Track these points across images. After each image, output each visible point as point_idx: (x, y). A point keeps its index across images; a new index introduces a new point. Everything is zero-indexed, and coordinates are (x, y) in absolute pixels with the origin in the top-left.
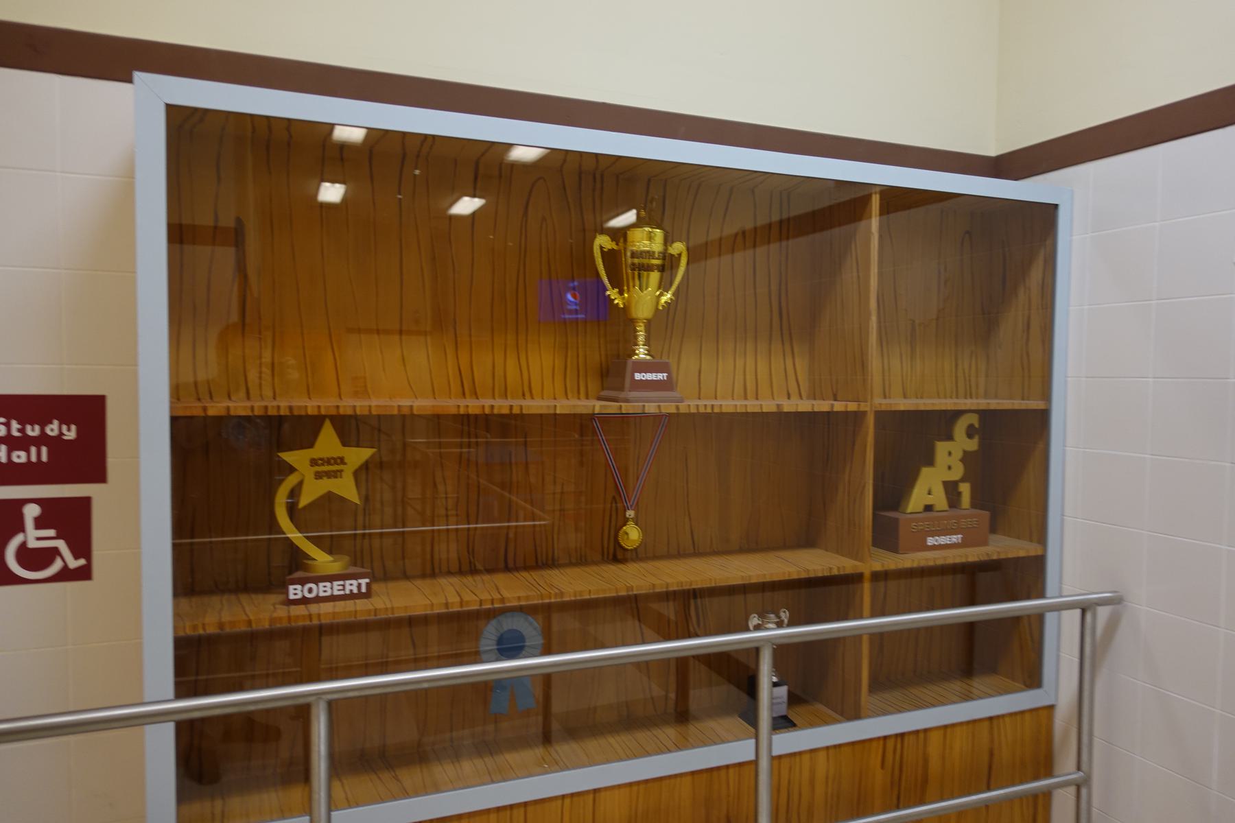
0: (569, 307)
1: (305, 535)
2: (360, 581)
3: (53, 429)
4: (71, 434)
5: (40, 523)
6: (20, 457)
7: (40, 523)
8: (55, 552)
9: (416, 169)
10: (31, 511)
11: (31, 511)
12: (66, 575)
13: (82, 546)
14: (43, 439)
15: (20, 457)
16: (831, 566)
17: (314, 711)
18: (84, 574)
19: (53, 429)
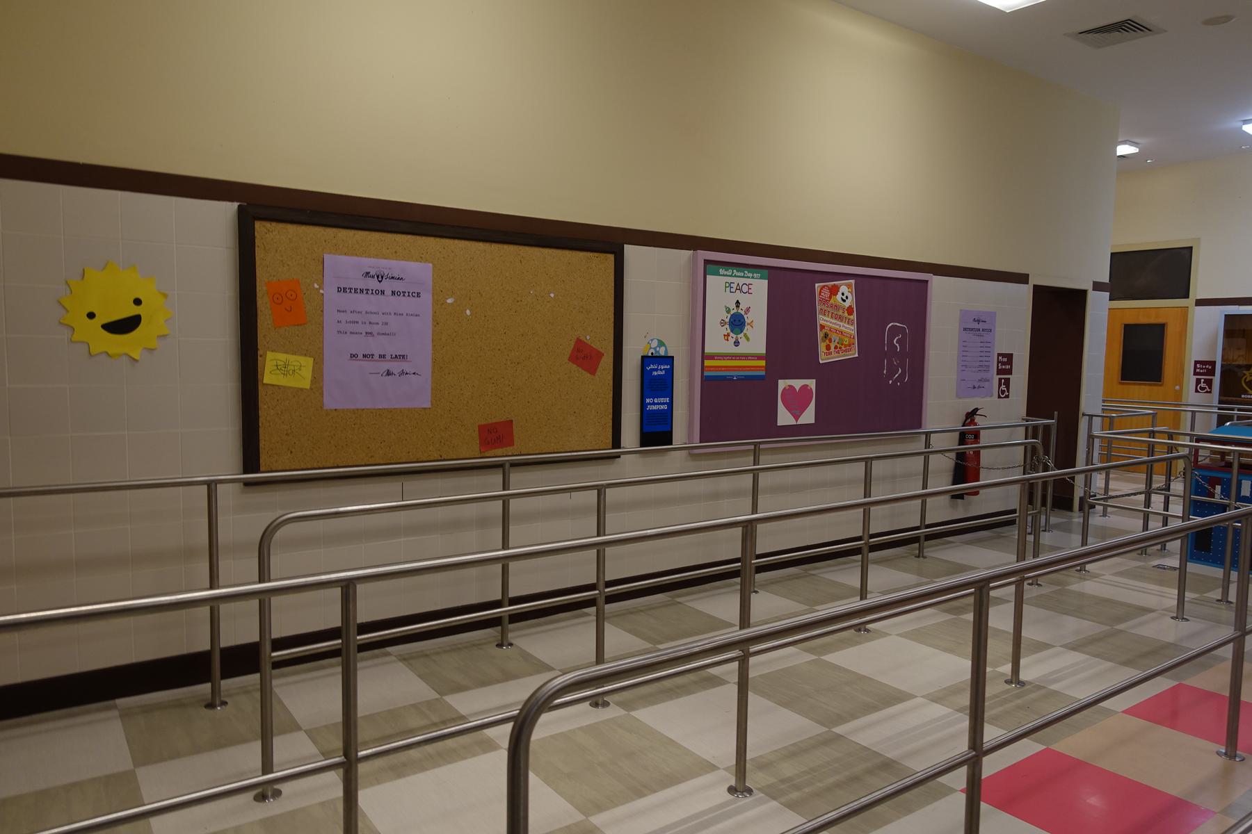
0: (1043, 518)
1: (783, 800)
2: (427, 298)
3: (1207, 367)
4: (1210, 368)
5: (1204, 383)
6: (1201, 371)
7: (1204, 383)
8: (1205, 388)
9: (1177, 385)
10: (1202, 380)
11: (1202, 380)
12: (1207, 392)
13: (1210, 388)
14: (1205, 368)
15: (1201, 371)
16: (1017, 522)
17: (1243, 462)
18: (1210, 392)
19: (1207, 367)
